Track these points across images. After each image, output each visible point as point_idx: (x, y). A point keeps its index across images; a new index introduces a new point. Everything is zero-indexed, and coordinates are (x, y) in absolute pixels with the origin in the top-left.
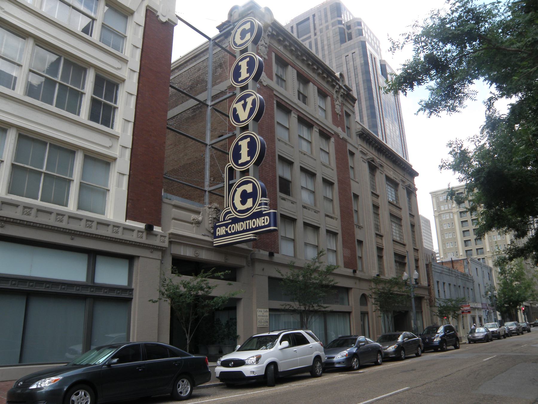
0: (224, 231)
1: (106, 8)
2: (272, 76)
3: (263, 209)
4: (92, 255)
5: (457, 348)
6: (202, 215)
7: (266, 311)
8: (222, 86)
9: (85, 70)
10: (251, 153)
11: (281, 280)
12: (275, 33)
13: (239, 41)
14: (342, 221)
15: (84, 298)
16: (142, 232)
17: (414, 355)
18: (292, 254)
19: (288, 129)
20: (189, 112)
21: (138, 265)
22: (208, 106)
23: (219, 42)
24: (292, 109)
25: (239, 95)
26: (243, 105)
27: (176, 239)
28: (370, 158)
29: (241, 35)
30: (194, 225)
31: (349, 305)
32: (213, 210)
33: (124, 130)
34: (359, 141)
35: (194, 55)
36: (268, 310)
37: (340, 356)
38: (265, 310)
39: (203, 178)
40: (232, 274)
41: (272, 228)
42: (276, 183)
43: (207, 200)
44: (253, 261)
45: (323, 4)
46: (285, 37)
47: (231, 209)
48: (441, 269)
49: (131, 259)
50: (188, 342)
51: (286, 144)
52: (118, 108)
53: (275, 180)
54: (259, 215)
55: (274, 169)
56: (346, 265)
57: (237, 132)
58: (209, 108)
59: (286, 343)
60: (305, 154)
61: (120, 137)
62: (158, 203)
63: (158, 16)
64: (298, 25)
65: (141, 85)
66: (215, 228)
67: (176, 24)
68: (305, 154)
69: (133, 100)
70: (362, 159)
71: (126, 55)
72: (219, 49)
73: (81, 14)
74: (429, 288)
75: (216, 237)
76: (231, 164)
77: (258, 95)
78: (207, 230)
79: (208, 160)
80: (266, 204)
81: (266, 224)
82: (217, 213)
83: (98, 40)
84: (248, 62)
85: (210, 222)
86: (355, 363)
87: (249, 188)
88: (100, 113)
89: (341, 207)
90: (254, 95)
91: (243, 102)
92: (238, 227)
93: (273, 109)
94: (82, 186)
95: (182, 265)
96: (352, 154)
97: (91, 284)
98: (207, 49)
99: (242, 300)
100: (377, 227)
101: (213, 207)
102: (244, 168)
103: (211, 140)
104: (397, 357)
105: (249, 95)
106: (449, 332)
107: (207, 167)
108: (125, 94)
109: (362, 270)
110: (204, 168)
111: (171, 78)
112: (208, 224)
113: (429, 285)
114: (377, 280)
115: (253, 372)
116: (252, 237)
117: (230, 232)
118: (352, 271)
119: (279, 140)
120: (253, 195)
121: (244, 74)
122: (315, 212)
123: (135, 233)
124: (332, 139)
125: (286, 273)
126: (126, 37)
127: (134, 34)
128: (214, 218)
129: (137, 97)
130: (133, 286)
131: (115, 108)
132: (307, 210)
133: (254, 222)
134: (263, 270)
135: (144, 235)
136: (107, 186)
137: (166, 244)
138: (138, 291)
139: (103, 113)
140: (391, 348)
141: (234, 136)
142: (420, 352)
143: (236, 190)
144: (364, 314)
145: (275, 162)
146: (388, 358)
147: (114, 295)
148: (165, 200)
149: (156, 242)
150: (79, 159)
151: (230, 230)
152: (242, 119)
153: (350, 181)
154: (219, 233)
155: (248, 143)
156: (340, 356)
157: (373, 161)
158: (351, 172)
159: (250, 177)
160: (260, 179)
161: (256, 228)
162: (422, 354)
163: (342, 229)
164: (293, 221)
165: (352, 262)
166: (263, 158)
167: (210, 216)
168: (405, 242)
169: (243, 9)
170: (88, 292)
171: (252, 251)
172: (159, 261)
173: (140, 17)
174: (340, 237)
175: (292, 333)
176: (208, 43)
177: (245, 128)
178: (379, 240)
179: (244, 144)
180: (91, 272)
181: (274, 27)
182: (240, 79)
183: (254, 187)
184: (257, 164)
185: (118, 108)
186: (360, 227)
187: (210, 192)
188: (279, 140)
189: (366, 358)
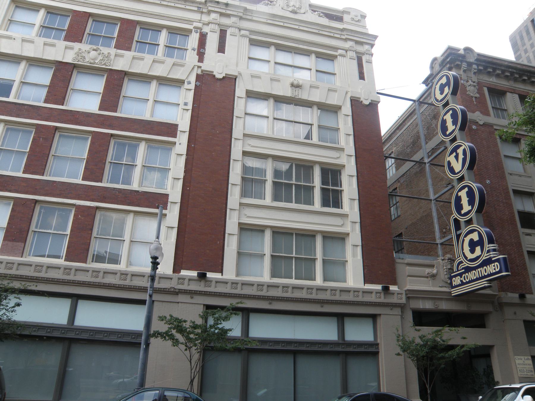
1: (319, 111)
3: (492, 256)
4: (341, 318)
6: (437, 268)
7: (528, 359)
8: (433, 144)
9: (312, 168)
10: (471, 202)
15: (337, 353)
21: (380, 321)
22: (425, 163)
24: (521, 137)
25: (450, 148)
26: (455, 156)
27: (411, 295)
29: (440, 90)
30: (429, 279)
32: (446, 261)
33: (351, 208)
36: (530, 358)
38: (526, 357)
39: (434, 232)
40: (477, 321)
43: (440, 252)
44: (501, 306)
46: (495, 66)
47: (462, 259)
49: (374, 317)
50: (429, 392)
51: (520, 176)
53: (514, 216)
54: (488, 262)
55: (510, 206)
57: (455, 183)
58: (427, 165)
61: (349, 217)
62: (392, 263)
66: (451, 278)
67: (379, 102)
72: (427, 105)
75: (453, 287)
76: (455, 215)
77: (466, 144)
79: (435, 214)
80: (494, 250)
81: (497, 270)
82: (451, 264)
83: (318, 140)
84: (451, 115)
85: (445, 273)
87: (475, 237)
91: (454, 154)
92: (471, 275)
93: (496, 145)
94: (324, 261)
95: (421, 318)
97: (342, 342)
98: (415, 110)
99: (495, 347)
101: (446, 258)
102: (467, 218)
103: (435, 194)
105: (459, 147)
107: (435, 220)
110: (433, 222)
111: (384, 149)
112: (443, 275)
116: (486, 285)
117: (464, 281)
119: (511, 174)
120: (480, 243)
121: (451, 127)
123: (374, 295)
127: (345, 124)
128: (449, 269)
129: (357, 176)
130: (379, 341)
134: (515, 313)
136: (345, 258)
137: (404, 301)
138: (383, 345)
139: (332, 198)
143: (463, 240)
145: (510, 199)
147: (362, 349)
148: (398, 261)
149: (394, 300)
150: (319, 241)
151: (465, 279)
152: (457, 171)
159: (475, 226)
160: (485, 226)
167: (445, 267)
169: (442, 58)
170: (340, 349)
171: (497, 295)
173: (347, 109)
176: (414, 105)
177: (461, 179)
179: (463, 194)
180: (341, 332)
181: (479, 63)
182: (448, 133)
183: (480, 235)
184: (479, 211)
187: (442, 244)
188: (511, 174)
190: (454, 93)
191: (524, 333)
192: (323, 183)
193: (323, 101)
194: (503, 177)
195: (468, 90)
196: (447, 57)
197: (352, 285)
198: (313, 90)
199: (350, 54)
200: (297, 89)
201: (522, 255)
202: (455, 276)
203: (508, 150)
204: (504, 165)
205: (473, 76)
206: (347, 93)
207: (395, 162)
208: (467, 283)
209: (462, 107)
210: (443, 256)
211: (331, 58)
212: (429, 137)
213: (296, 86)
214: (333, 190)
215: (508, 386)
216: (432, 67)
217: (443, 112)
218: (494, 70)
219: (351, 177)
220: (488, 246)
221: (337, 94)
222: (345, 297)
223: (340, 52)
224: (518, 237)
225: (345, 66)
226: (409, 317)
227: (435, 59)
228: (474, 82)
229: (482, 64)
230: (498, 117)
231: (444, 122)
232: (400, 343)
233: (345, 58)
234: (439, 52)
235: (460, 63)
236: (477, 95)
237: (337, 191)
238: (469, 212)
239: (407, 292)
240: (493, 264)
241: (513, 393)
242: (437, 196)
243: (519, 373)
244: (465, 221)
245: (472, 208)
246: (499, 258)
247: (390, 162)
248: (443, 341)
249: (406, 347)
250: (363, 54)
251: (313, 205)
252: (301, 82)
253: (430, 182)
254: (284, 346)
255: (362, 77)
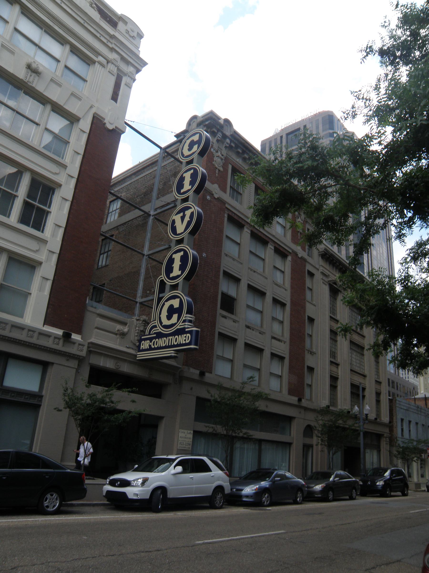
0: (148, 345)
2: (226, 188)
3: (186, 326)
5: (404, 495)
6: (129, 327)
7: (190, 433)
8: (168, 198)
10: (182, 268)
11: (209, 400)
12: (233, 145)
13: (186, 152)
14: (290, 345)
16: (59, 339)
17: (348, 497)
18: (228, 375)
19: (239, 244)
20: (139, 219)
21: (51, 372)
23: (173, 152)
27: (94, 349)
28: (333, 280)
30: (118, 336)
31: (290, 435)
32: (141, 322)
33: (54, 235)
34: (321, 262)
35: (152, 162)
36: (192, 432)
37: (249, 490)
38: (189, 432)
40: (153, 389)
41: (192, 346)
42: (217, 300)
43: (137, 311)
45: (315, 115)
46: (245, 149)
47: (157, 323)
48: (407, 405)
51: (234, 259)
52: (51, 212)
53: (217, 296)
55: (216, 285)
56: (291, 392)
57: (173, 244)
58: (151, 218)
59: (179, 469)
60: (255, 272)
63: (105, 124)
64: (288, 134)
65: (77, 191)
66: (140, 341)
67: (123, 132)
68: (255, 272)
69: (67, 205)
70: (322, 281)
71: (66, 160)
72: (172, 159)
73: (25, 119)
74: (390, 426)
75: (140, 351)
76: (163, 277)
77: (196, 208)
78: (132, 342)
80: (190, 321)
81: (187, 342)
82: (145, 326)
84: (191, 174)
85: (136, 334)
86: (265, 498)
87: (176, 303)
88: (32, 215)
89: (292, 329)
90: (193, 209)
91: (182, 214)
92: (161, 342)
95: (98, 376)
96: (311, 275)
99: (165, 419)
100: (333, 354)
101: (141, 319)
102: (174, 282)
103: (149, 250)
104: (323, 497)
105: (188, 208)
106: (395, 477)
107: (142, 277)
108: (59, 199)
109: (311, 400)
112: (133, 336)
113: (390, 422)
114: (325, 411)
115: (137, 495)
116: (173, 354)
117: (153, 347)
118: (296, 399)
119: (226, 255)
121: (187, 186)
122: (260, 333)
124: (289, 258)
125: (215, 394)
126: (69, 142)
127: (78, 142)
128: (141, 331)
129: (72, 202)
130: (44, 393)
131: (48, 213)
132: (251, 331)
133: (176, 339)
134: (191, 389)
135: (61, 342)
136: (30, 290)
137: (83, 353)
139: (34, 216)
140: (318, 487)
141: (170, 247)
142: (354, 495)
143: (164, 304)
144: (307, 448)
145: (219, 278)
146: (310, 497)
147: (22, 400)
148: (90, 308)
149: (73, 350)
151: (154, 345)
152: (178, 232)
153: (305, 303)
154: (143, 347)
155: (182, 257)
156: (249, 490)
157: (335, 283)
158: (308, 293)
159: (178, 292)
160: (189, 294)
161: (178, 345)
162: (357, 497)
163: (290, 353)
164: (233, 340)
165: (297, 389)
166: (194, 273)
167: (137, 328)
168: (366, 373)
169: (202, 119)
171: (180, 368)
172: (75, 370)
173: (85, 124)
174: (287, 361)
175: (192, 459)
177: (180, 242)
178: (334, 369)
179: (177, 257)
181: (233, 139)
182: (182, 191)
183: (181, 303)
184: (187, 278)
185: (51, 212)
186: (312, 353)
187: (141, 303)
188: (226, 255)
189: (281, 494)
190: (202, 153)
191: (194, 408)
192: (29, 196)
193: (61, 103)
194: (219, 255)
195: (215, 159)
196: (207, 120)
197: (29, 322)
198: (54, 85)
199: (111, 67)
200: (34, 75)
201: (213, 335)
202: (145, 340)
203: (229, 231)
204: (223, 244)
205: (224, 149)
206: (91, 107)
207: (121, 207)
208: (155, 349)
209: (205, 171)
210: (139, 317)
211: (88, 61)
212: (163, 192)
213: (31, 69)
214: (38, 208)
215: (165, 457)
216: (189, 124)
217: (184, 169)
218: (244, 152)
219: (64, 201)
220: (185, 316)
221: (80, 102)
222: (16, 335)
223: (100, 59)
224: (214, 316)
225: (100, 78)
226: (86, 373)
227: (195, 117)
228: (222, 155)
229: (235, 141)
230: (233, 197)
231: (182, 179)
232: (67, 398)
233: (103, 69)
234: (200, 113)
235: (216, 131)
236: (221, 169)
237: (44, 211)
238: (178, 277)
239: (90, 345)
240: (185, 335)
241: (168, 464)
242: (151, 252)
243: (179, 446)
244: (171, 285)
245: (182, 273)
246: (192, 331)
247: (117, 205)
248: (112, 402)
249: (72, 403)
250: (125, 75)
251: (9, 217)
252: (41, 69)
253: (149, 235)
254: (27, 399)
255: (115, 97)
